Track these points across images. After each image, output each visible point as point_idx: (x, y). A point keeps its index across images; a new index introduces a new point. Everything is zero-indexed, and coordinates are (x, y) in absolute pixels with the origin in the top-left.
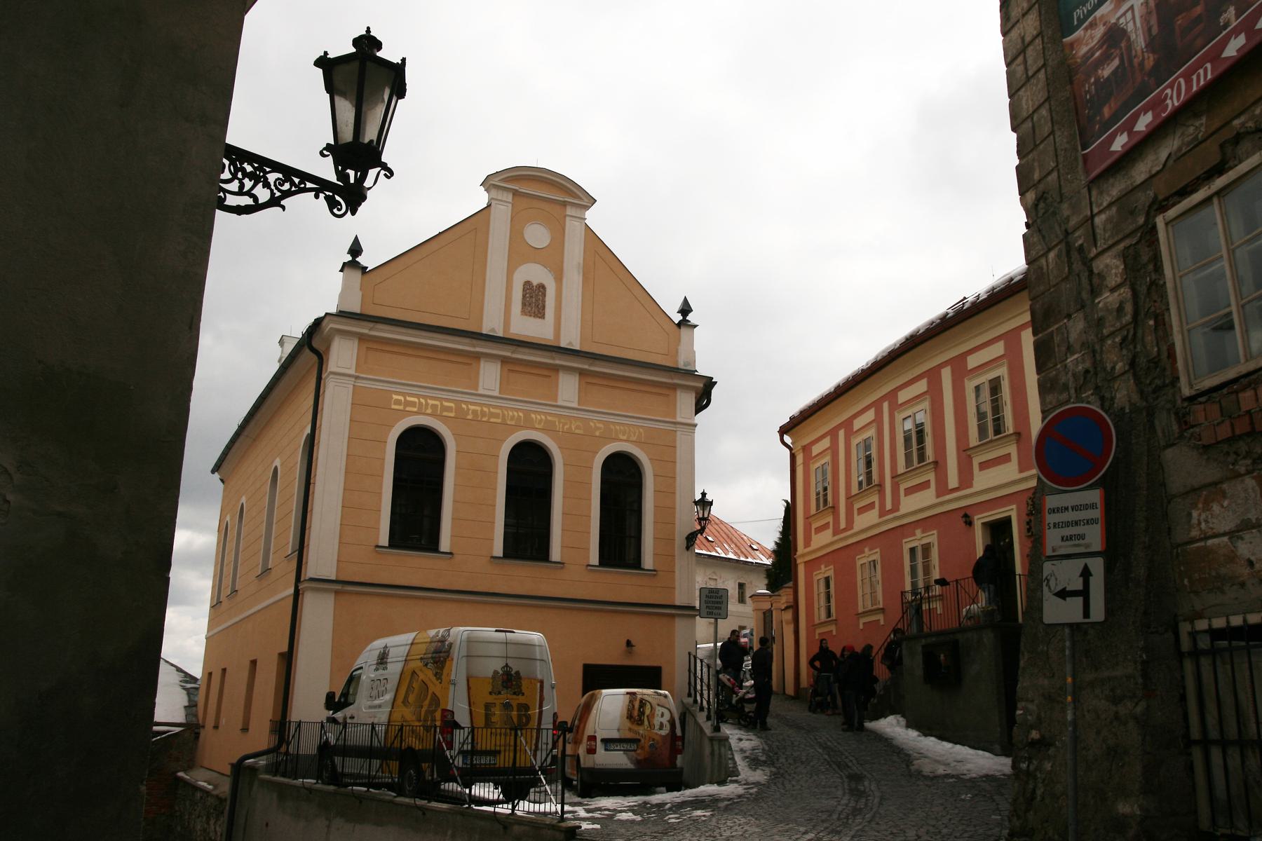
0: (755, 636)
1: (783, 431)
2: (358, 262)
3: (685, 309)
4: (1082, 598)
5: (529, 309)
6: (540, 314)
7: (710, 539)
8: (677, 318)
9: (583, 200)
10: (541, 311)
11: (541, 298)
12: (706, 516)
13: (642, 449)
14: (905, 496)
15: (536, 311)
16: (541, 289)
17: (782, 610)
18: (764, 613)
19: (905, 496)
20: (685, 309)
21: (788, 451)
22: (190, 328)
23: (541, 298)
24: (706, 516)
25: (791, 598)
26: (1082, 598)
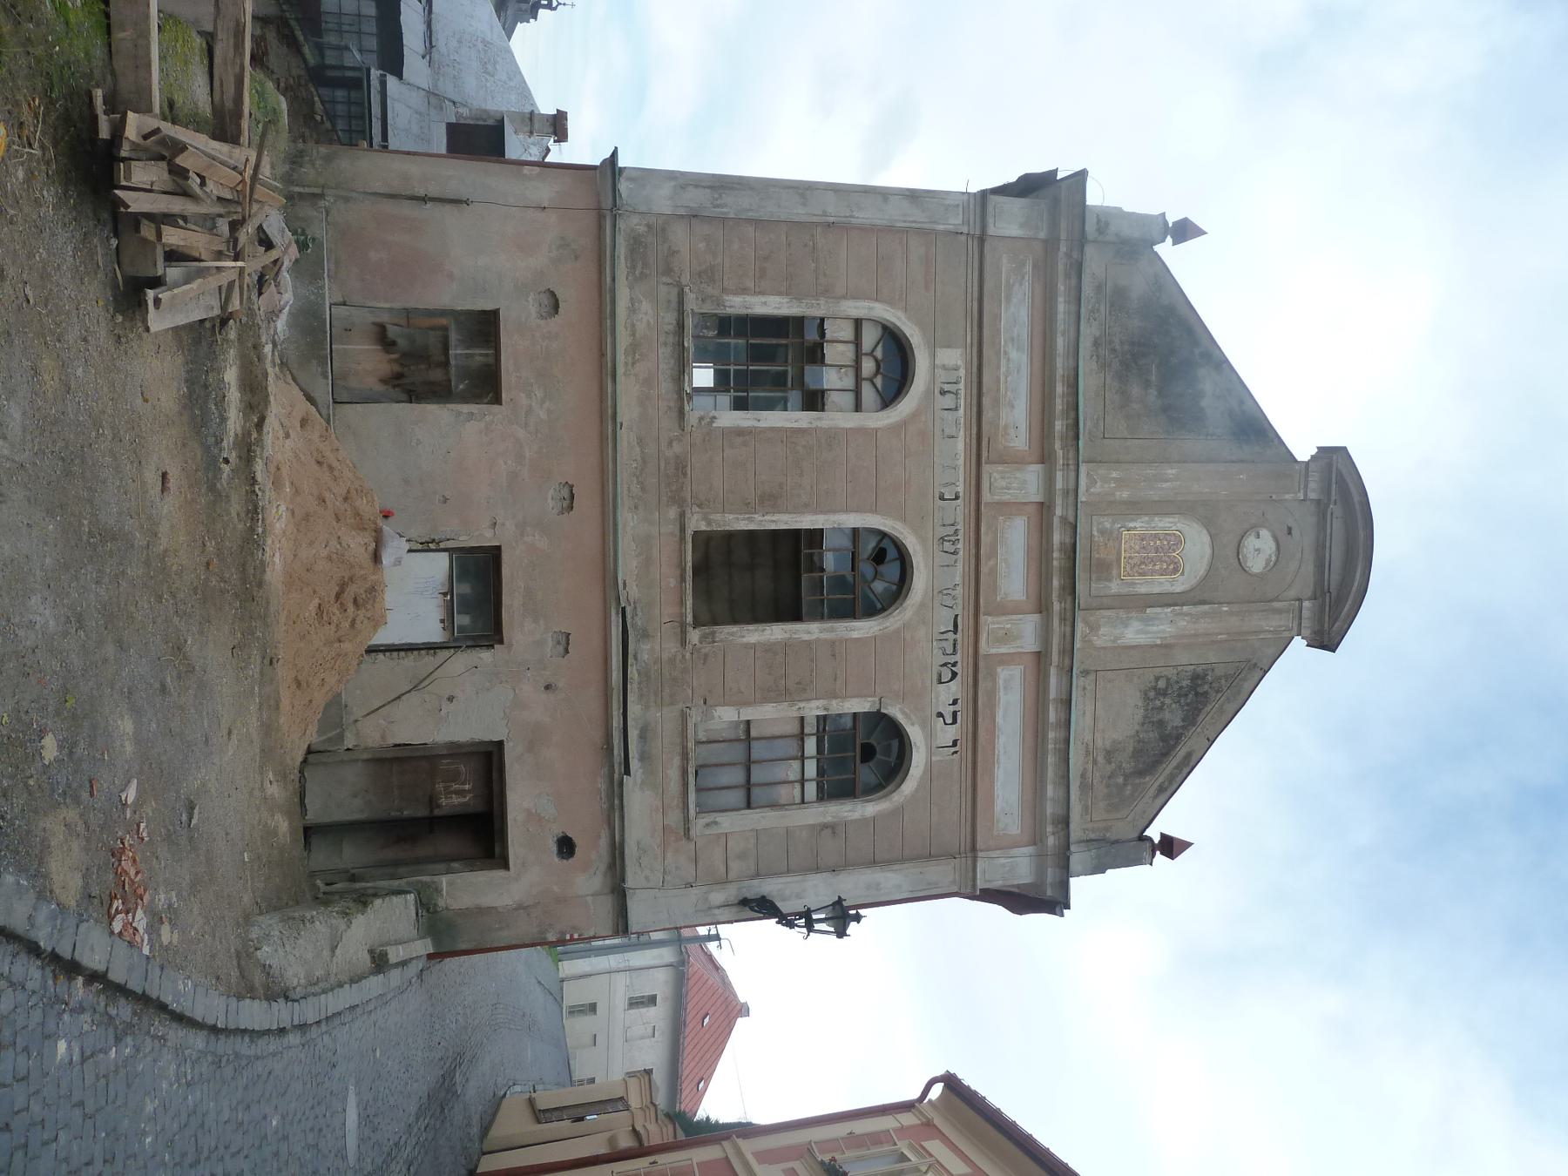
0: (1160, 780)
1: (951, 1083)
2: (1156, 253)
3: (1171, 847)
4: (712, 385)
5: (1137, 547)
6: (1131, 569)
7: (706, 1021)
8: (1154, 832)
9: (1326, 640)
10: (1137, 568)
11: (1157, 567)
12: (817, 926)
13: (922, 778)
14: (783, 1170)
15: (1135, 561)
16: (1172, 567)
17: (633, 1126)
18: (622, 1098)
19: (783, 1170)
20: (1171, 847)
21: (915, 1095)
22: (744, 902)
23: (1157, 567)
24: (817, 926)
25: (655, 1140)
26: (712, 385)
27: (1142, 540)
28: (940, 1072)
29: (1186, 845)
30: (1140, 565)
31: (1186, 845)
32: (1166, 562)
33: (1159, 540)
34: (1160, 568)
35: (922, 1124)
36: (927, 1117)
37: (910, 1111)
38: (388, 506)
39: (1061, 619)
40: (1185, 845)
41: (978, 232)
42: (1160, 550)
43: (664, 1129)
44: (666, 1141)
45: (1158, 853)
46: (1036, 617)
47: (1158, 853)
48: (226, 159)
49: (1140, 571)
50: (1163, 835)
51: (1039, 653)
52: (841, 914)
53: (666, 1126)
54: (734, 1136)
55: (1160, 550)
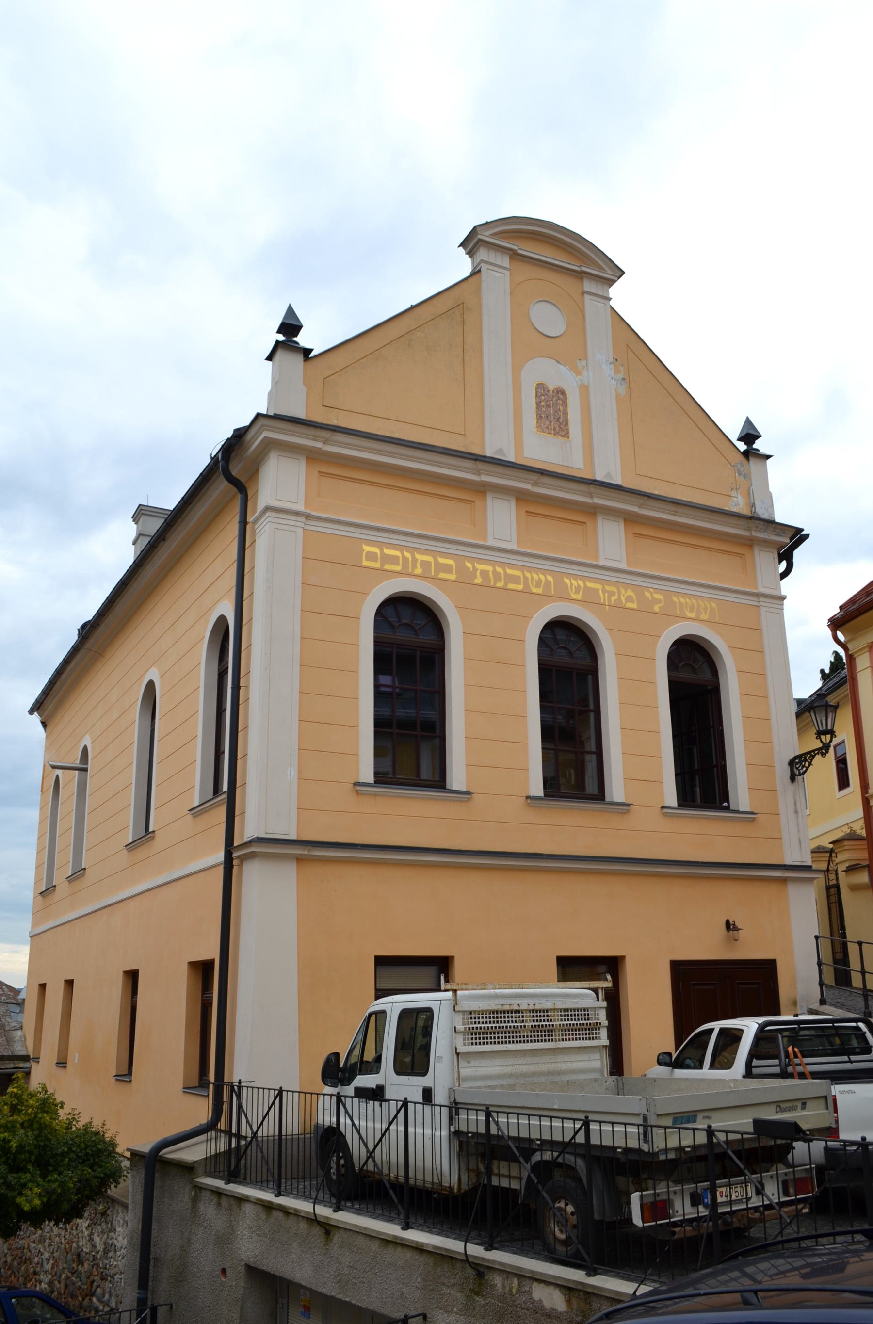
5: (547, 423)
10: (562, 426)
11: (561, 408)
16: (560, 396)
27: (541, 417)
28: (829, 632)
29: (290, 311)
30: (560, 423)
31: (290, 311)
32: (557, 400)
33: (541, 402)
34: (562, 406)
35: (870, 651)
36: (866, 646)
37: (855, 659)
38: (61, 1071)
39: (675, 515)
40: (290, 311)
41: (303, 520)
42: (548, 403)
43: (846, 848)
44: (866, 847)
45: (295, 339)
46: (756, 550)
47: (295, 339)
48: (347, 1218)
49: (564, 423)
50: (279, 332)
51: (517, 499)
52: (824, 707)
53: (845, 845)
54: (866, 795)
55: (548, 403)
